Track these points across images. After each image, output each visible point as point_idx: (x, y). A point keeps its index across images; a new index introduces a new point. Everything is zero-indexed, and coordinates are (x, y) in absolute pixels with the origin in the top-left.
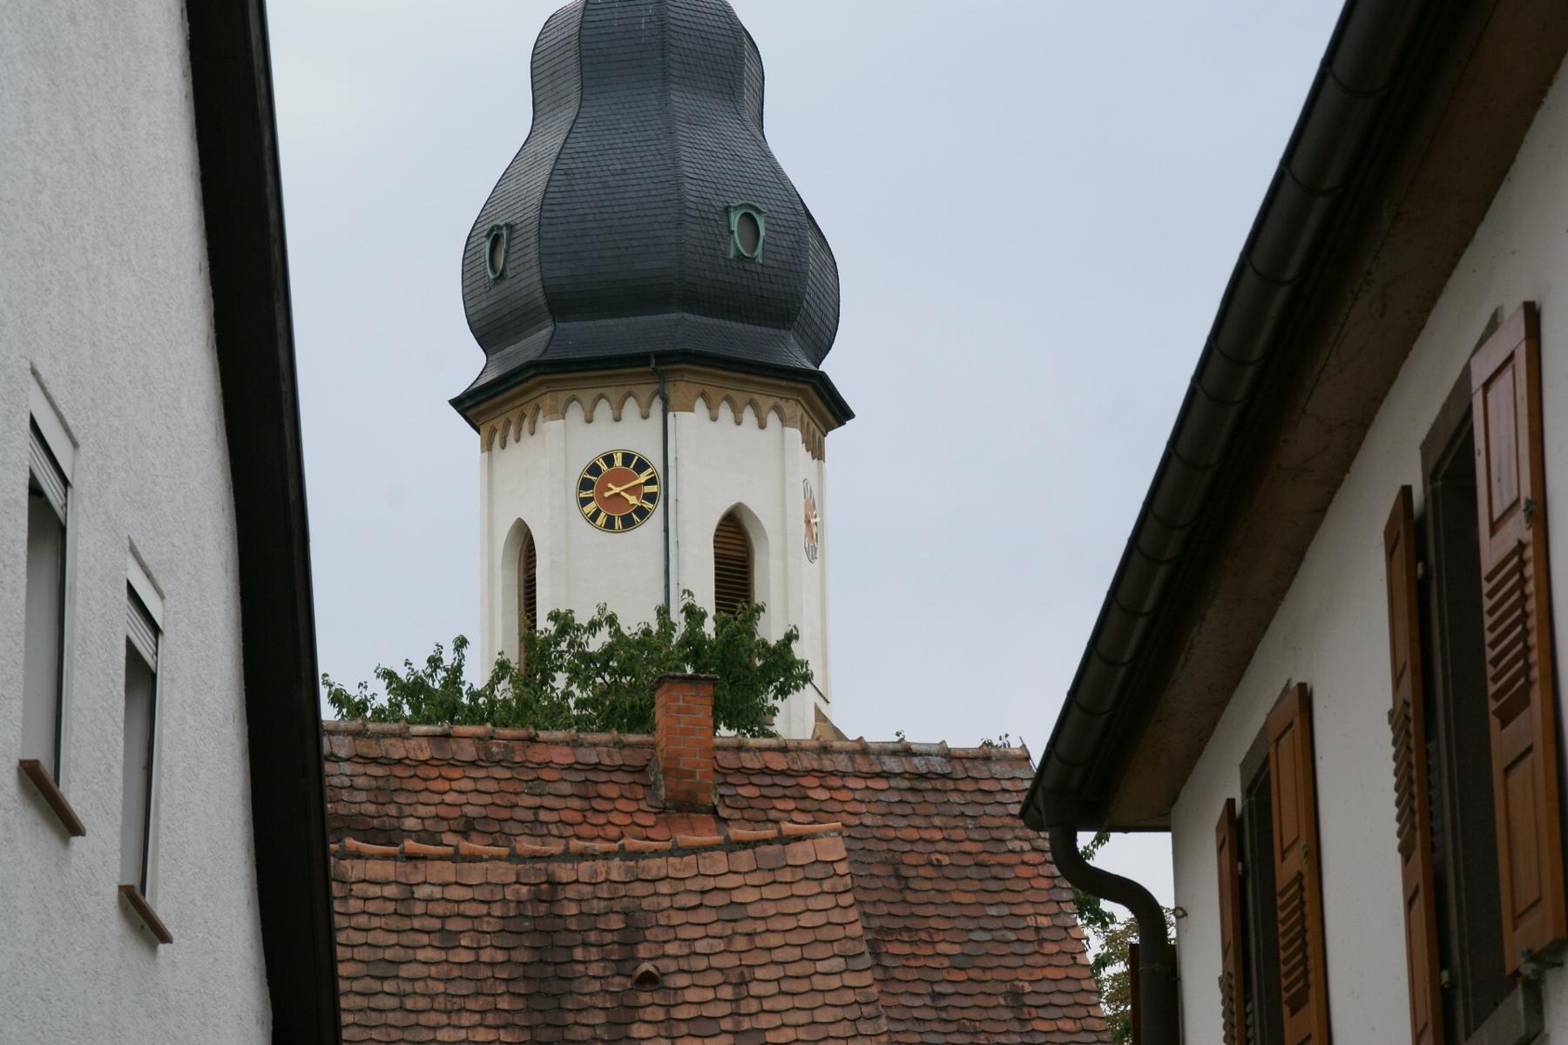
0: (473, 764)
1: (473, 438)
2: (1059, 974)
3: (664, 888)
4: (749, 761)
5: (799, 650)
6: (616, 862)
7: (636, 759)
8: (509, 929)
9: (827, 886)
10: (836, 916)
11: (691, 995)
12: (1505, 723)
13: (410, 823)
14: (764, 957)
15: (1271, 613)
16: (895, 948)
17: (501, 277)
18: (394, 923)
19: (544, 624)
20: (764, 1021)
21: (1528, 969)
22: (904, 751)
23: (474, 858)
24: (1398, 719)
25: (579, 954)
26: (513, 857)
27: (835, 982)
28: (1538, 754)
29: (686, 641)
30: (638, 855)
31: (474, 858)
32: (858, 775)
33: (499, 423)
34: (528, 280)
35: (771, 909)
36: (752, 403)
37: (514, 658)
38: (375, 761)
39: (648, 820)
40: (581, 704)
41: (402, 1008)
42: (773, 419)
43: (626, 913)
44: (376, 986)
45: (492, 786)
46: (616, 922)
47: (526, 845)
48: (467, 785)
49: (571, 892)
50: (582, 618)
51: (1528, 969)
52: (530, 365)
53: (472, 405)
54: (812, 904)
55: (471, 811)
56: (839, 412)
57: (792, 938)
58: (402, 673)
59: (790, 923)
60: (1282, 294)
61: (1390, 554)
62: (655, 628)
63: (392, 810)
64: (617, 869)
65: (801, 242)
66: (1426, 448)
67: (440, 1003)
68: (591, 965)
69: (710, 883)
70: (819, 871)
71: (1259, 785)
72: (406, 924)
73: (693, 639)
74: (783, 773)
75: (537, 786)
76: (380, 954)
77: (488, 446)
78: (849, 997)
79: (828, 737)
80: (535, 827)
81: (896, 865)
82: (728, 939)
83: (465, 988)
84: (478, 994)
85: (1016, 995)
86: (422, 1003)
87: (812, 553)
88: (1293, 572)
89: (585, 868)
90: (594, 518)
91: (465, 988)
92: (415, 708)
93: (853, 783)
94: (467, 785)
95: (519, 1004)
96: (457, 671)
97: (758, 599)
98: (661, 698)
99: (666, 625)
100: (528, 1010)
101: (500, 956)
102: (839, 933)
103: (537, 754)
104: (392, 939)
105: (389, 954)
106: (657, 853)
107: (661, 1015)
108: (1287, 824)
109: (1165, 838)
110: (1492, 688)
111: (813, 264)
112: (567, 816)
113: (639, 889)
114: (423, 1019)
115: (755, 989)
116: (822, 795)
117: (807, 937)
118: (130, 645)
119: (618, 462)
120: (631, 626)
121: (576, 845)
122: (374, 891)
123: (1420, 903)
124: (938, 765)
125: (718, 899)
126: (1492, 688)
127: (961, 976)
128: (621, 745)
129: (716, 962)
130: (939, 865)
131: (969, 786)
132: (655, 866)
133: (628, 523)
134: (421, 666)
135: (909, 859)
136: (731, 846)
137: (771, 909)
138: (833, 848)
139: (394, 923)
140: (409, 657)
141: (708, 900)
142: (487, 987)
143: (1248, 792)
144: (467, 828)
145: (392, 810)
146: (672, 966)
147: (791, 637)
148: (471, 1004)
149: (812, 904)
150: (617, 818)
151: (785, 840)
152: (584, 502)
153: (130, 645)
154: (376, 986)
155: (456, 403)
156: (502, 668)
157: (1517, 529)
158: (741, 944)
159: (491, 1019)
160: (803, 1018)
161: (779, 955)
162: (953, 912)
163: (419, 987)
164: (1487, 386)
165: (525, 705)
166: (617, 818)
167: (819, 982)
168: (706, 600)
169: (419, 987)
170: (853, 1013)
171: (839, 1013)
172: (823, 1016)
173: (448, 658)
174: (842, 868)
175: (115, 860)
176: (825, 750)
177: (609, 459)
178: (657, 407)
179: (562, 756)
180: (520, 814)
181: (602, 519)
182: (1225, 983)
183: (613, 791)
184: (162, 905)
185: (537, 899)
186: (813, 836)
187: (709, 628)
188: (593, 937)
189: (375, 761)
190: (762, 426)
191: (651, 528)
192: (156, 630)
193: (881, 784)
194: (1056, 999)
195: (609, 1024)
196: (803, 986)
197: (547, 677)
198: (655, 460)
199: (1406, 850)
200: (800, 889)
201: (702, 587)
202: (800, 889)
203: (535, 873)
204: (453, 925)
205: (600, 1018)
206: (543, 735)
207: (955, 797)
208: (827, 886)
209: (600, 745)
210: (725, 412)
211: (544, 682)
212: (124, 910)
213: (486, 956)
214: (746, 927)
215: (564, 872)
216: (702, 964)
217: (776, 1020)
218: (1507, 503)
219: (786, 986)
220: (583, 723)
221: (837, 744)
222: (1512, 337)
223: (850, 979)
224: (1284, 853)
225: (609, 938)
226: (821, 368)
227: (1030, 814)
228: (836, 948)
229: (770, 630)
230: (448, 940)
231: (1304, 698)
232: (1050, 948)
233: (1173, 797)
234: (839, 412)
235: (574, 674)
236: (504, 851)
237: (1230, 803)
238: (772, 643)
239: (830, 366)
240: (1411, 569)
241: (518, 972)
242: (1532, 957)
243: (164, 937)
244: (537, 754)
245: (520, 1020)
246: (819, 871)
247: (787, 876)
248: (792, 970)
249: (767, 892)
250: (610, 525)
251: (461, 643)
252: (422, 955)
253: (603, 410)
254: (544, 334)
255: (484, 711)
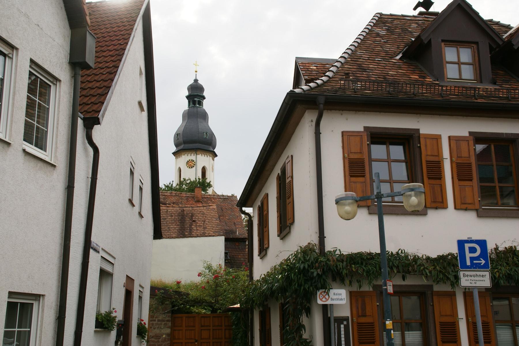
0: (174, 196)
1: (175, 157)
2: (240, 221)
3: (196, 211)
4: (205, 196)
5: (211, 183)
6: (191, 208)
7: (193, 196)
8: (178, 215)
9: (214, 211)
10: (215, 214)
11: (199, 223)
12: (288, 199)
13: (167, 202)
14: (207, 219)
15: (264, 185)
16: (222, 218)
17: (178, 139)
18: (166, 214)
19: (182, 179)
20: (207, 226)
21: (289, 225)
22: (223, 196)
23: (175, 207)
24: (277, 198)
25: (186, 218)
26: (179, 207)
27: (215, 222)
28: (291, 203)
29: (198, 182)
30: (193, 207)
31: (175, 207)
32: (218, 198)
33: (177, 156)
34: (181, 140)
35: (208, 213)
36: (206, 154)
37: (179, 183)
38: (164, 195)
39: (194, 203)
40: (186, 189)
41: (166, 223)
42: (208, 156)
43: (192, 214)
44: (164, 221)
45: (177, 199)
46: (190, 215)
47: (180, 205)
48: (174, 198)
49: (185, 211)
50: (187, 179)
51: (289, 225)
52: (181, 149)
53: (174, 154)
54: (213, 213)
55: (174, 201)
56: (216, 156)
57: (210, 217)
58: (166, 185)
59: (210, 215)
60: (266, 152)
61: (277, 180)
62: (195, 180)
63: (165, 201)
64: (191, 209)
65: (212, 136)
66: (281, 169)
67: (171, 223)
68: (188, 220)
69: (201, 211)
70: (213, 209)
71: (262, 203)
72: (167, 214)
73: (199, 182)
74: (210, 198)
75: (182, 199)
76: (164, 217)
77: (176, 158)
78: (216, 223)
79: (215, 194)
80: (181, 203)
81: (222, 208)
82: (203, 217)
83: (174, 221)
84: (175, 222)
85: (235, 223)
86: (169, 223)
87: (213, 171)
88: (267, 181)
89: (187, 208)
90: (188, 167)
91: (174, 221)
92: (168, 189)
93: (217, 199)
94: (174, 198)
95: (179, 223)
96: (172, 184)
97: (206, 177)
98: (196, 189)
99: (196, 180)
100: (181, 224)
101: (177, 218)
102: (215, 216)
103: (182, 195)
104: (165, 216)
105: (165, 217)
106: (195, 207)
107: (195, 225)
108: (265, 208)
109: (252, 208)
110: (287, 195)
111: (213, 139)
112: (185, 202)
113: (193, 211)
114: (169, 225)
115: (206, 222)
116: (214, 200)
117: (212, 217)
118: (140, 186)
119: (191, 160)
120: (192, 180)
121: (186, 206)
122: (163, 210)
123: (279, 218)
124: (227, 197)
125: (202, 212)
126: (287, 195)
127: (228, 221)
128: (191, 194)
129: (202, 219)
130: (226, 209)
131: (230, 200)
132: (195, 208)
133: (192, 167)
134: (168, 184)
135: (223, 208)
136: (203, 206)
137: (208, 213)
138: (215, 207)
139: (166, 214)
140: (167, 183)
141: (201, 212)
142: (176, 221)
143: (261, 204)
144: (174, 203)
145: (165, 201)
146: (197, 219)
147: (210, 182)
148: (174, 223)
149: (213, 213)
150: (190, 202)
151: (210, 206)
152: (187, 165)
153: (140, 186)
154: (164, 221)
155: (172, 153)
156: (178, 184)
157: (290, 179)
158: (204, 217)
159: (176, 225)
160: (211, 226)
161: (209, 219)
162: (228, 214)
163: (168, 221)
164: (287, 163)
165: (180, 189)
166: (190, 202)
167: (213, 222)
168: (201, 177)
169: (168, 221)
170: (216, 225)
171: (215, 225)
172: (213, 225)
173: (171, 183)
174: (216, 209)
175: (138, 209)
176: (214, 195)
177: (190, 160)
178: (195, 154)
179: (184, 195)
180: (180, 202)
181: (189, 167)
182: (258, 224)
183: (190, 200)
184: (143, 214)
185: (182, 212)
186: (213, 205)
187: (201, 180)
188: (188, 216)
189: (164, 195)
190: (207, 157)
191: (194, 168)
192: (142, 184)
193: (220, 199)
194: (239, 224)
195: (190, 226)
196: (211, 222)
197: (182, 186)
198: (195, 160)
199: (277, 212)
200: (211, 211)
201: (200, 175)
202: (211, 211)
203: (181, 209)
204: (172, 214)
205: (188, 225)
206: (182, 193)
207: (228, 201)
208: (214, 211)
209: (189, 194)
210: (203, 155)
211: (182, 186)
212: (139, 214)
213: (176, 218)
214: (205, 215)
215: (185, 209)
216: (200, 219)
217: (208, 226)
218: (289, 176)
219: (209, 222)
220: (186, 191)
221: (215, 195)
222: (290, 159)
223: (216, 221)
224: (265, 245)
225: (190, 216)
226: (215, 150)
227: (237, 205)
228: (215, 218)
229: (208, 181)
230: (172, 216)
231: (267, 195)
232: (239, 218)
233: (253, 204)
234: (216, 156)
235: (186, 185)
236: (178, 206)
237: (259, 205)
238: (208, 182)
239: (215, 150)
240: (279, 182)
241: (179, 220)
242: (290, 224)
243: (143, 217)
244: (182, 195)
245: (180, 225)
246: (213, 209)
247: (210, 210)
248: (210, 220)
249: (207, 212)
250: (190, 168)
251: (173, 181)
252: (169, 218)
253: (189, 155)
254: (183, 146)
255: (176, 190)
